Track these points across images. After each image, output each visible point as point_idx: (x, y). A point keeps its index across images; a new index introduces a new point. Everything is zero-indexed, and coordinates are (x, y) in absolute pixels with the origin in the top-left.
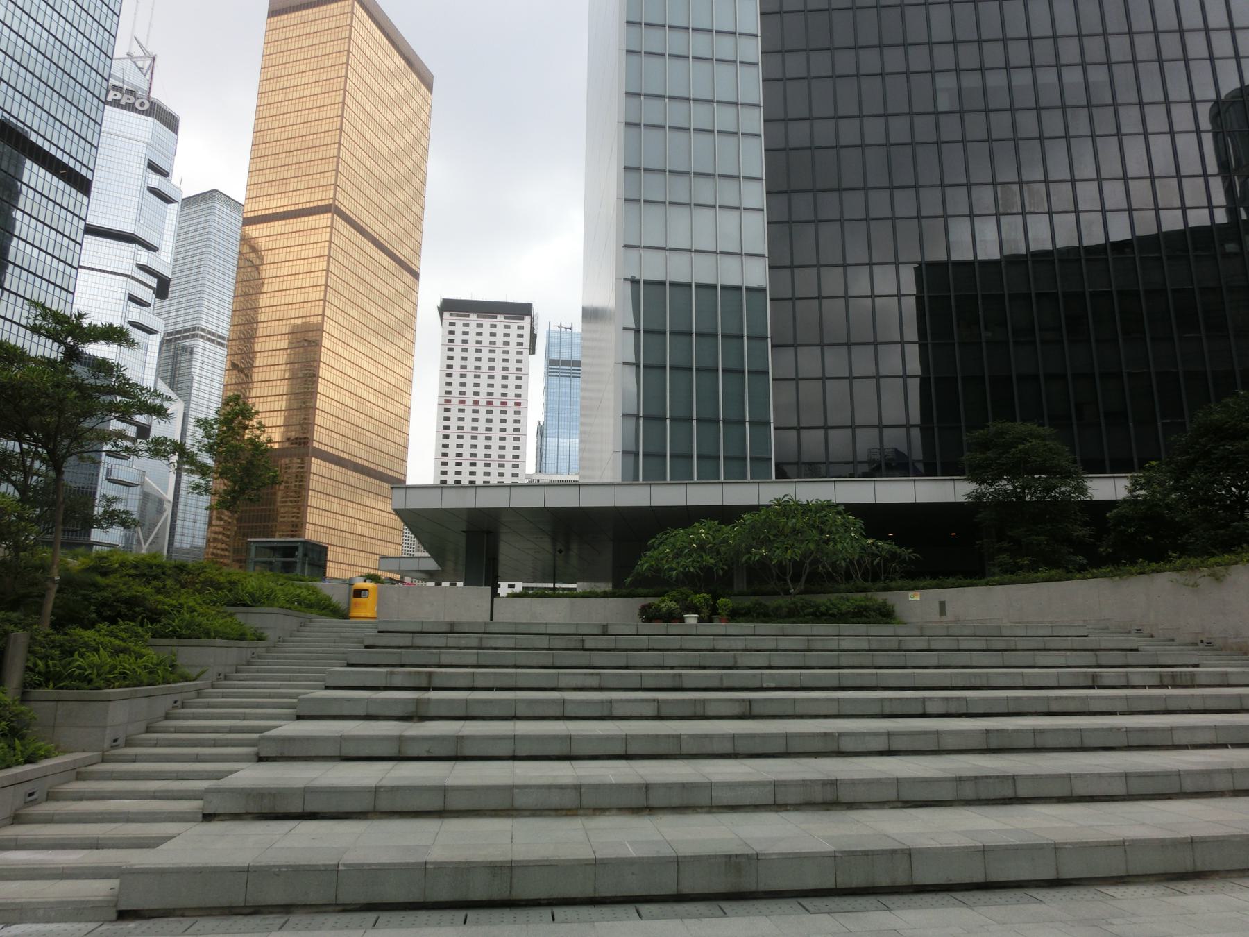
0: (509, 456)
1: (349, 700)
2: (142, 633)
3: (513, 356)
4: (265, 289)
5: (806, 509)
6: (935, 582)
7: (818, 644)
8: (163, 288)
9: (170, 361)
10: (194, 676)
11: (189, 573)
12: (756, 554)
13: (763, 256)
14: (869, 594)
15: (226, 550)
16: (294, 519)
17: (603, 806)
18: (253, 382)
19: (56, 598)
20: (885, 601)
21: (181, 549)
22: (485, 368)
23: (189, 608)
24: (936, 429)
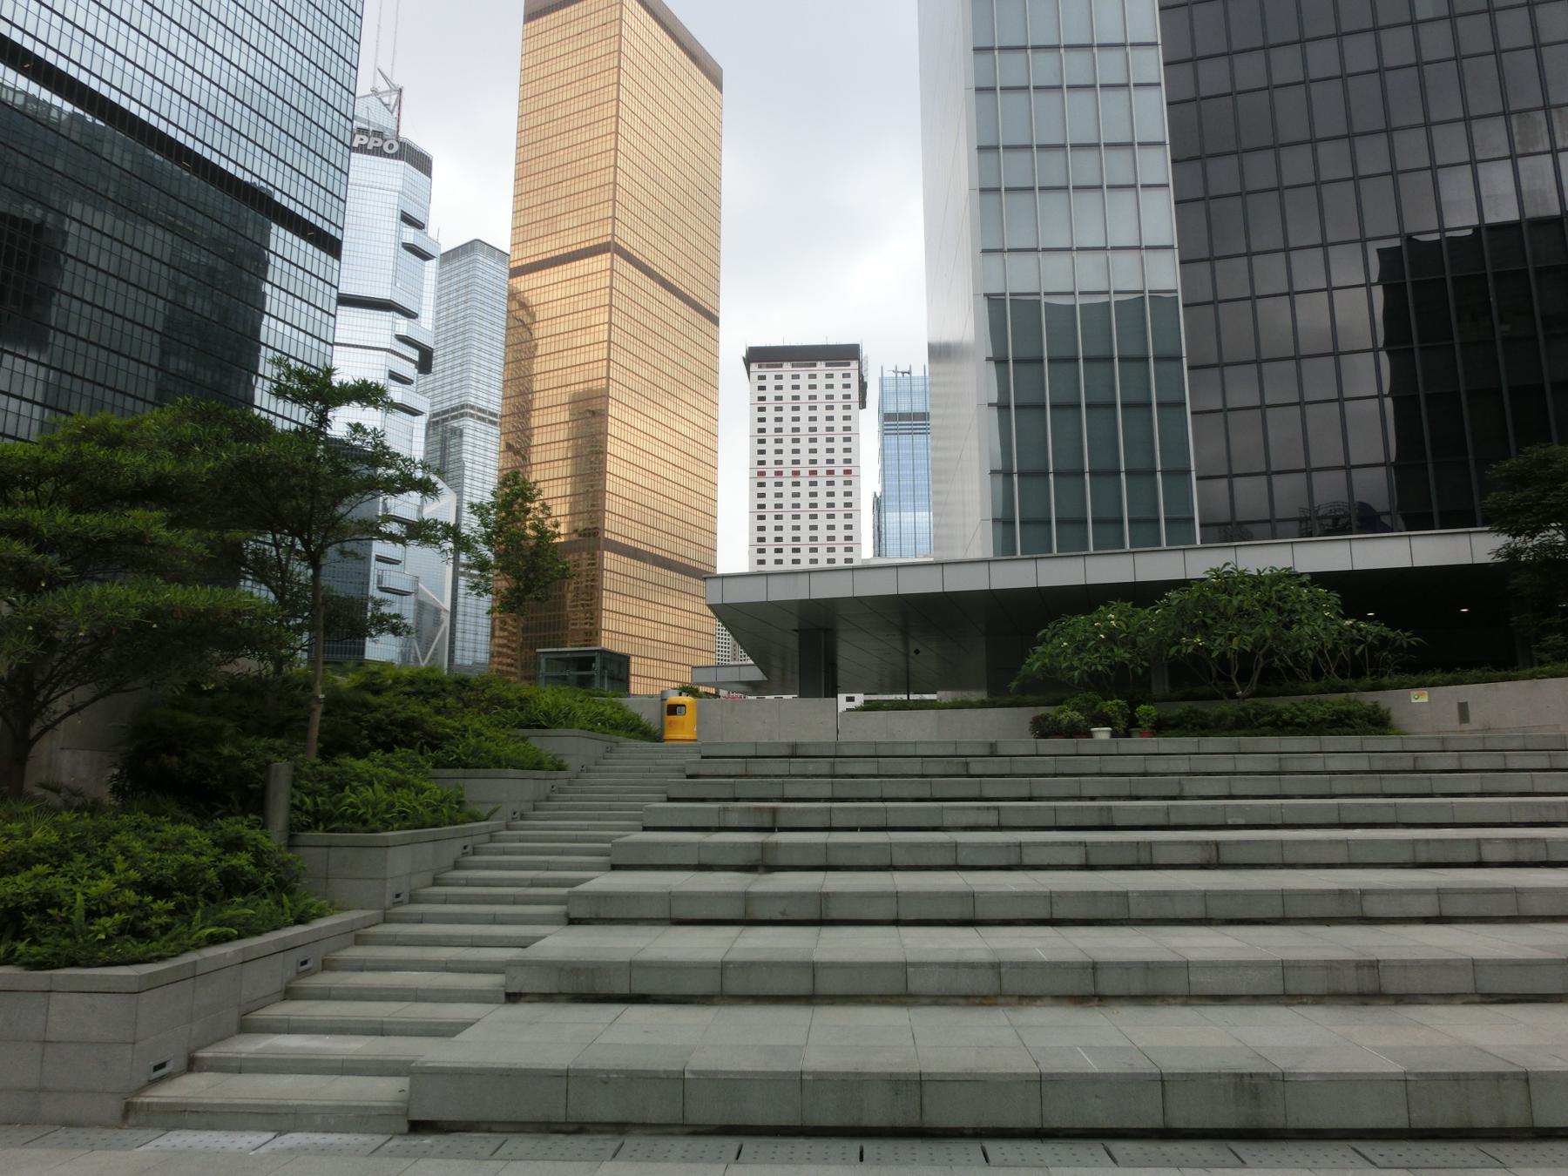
0: (840, 538)
1: (675, 845)
2: (422, 762)
3: (838, 413)
4: (539, 352)
5: (1257, 581)
6: (1449, 677)
7: (1295, 765)
8: (425, 362)
9: (438, 446)
10: (485, 815)
11: (472, 689)
12: (1187, 645)
13: (1172, 247)
14: (1352, 695)
15: (512, 665)
16: (587, 627)
17: (1033, 993)
18: (531, 465)
19: (321, 721)
20: (1376, 705)
21: (462, 666)
22: (804, 429)
23: (475, 731)
24: (1430, 467)
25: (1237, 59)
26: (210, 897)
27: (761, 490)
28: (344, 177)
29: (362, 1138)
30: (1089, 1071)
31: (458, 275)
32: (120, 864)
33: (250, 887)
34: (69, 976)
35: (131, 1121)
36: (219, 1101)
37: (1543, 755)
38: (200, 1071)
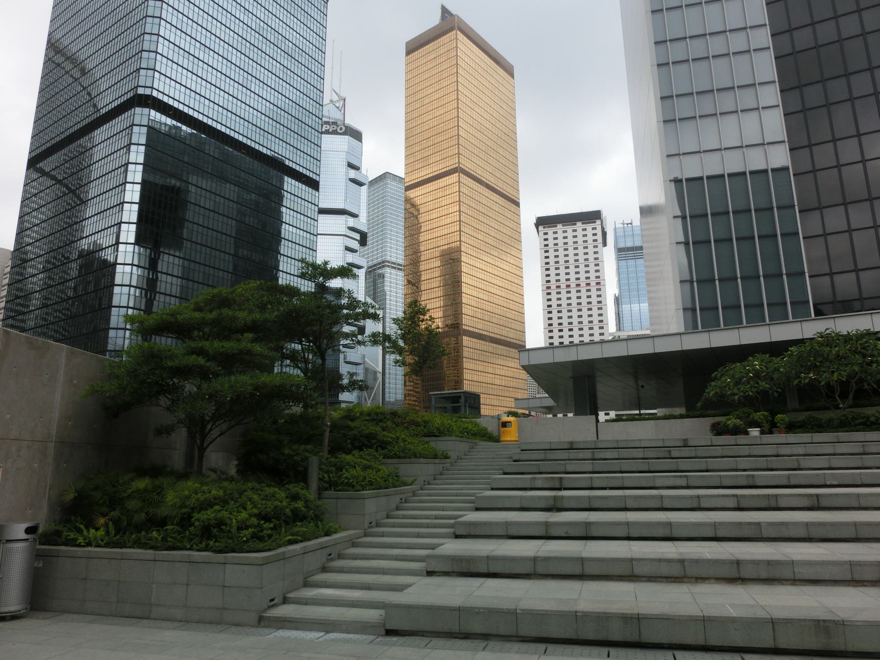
0: (596, 322)
2: (378, 456)
3: (591, 250)
5: (847, 338)
8: (363, 241)
9: (372, 284)
11: (399, 417)
12: (805, 378)
13: (784, 142)
18: (421, 291)
19: (330, 436)
21: (389, 402)
23: (402, 439)
25: (818, 26)
26: (287, 523)
27: (549, 297)
28: (319, 148)
29: (365, 637)
30: (731, 616)
31: (378, 192)
32: (249, 506)
33: (303, 518)
34: (233, 557)
35: (262, 624)
36: (298, 617)
37: (830, 446)
38: (289, 603)
